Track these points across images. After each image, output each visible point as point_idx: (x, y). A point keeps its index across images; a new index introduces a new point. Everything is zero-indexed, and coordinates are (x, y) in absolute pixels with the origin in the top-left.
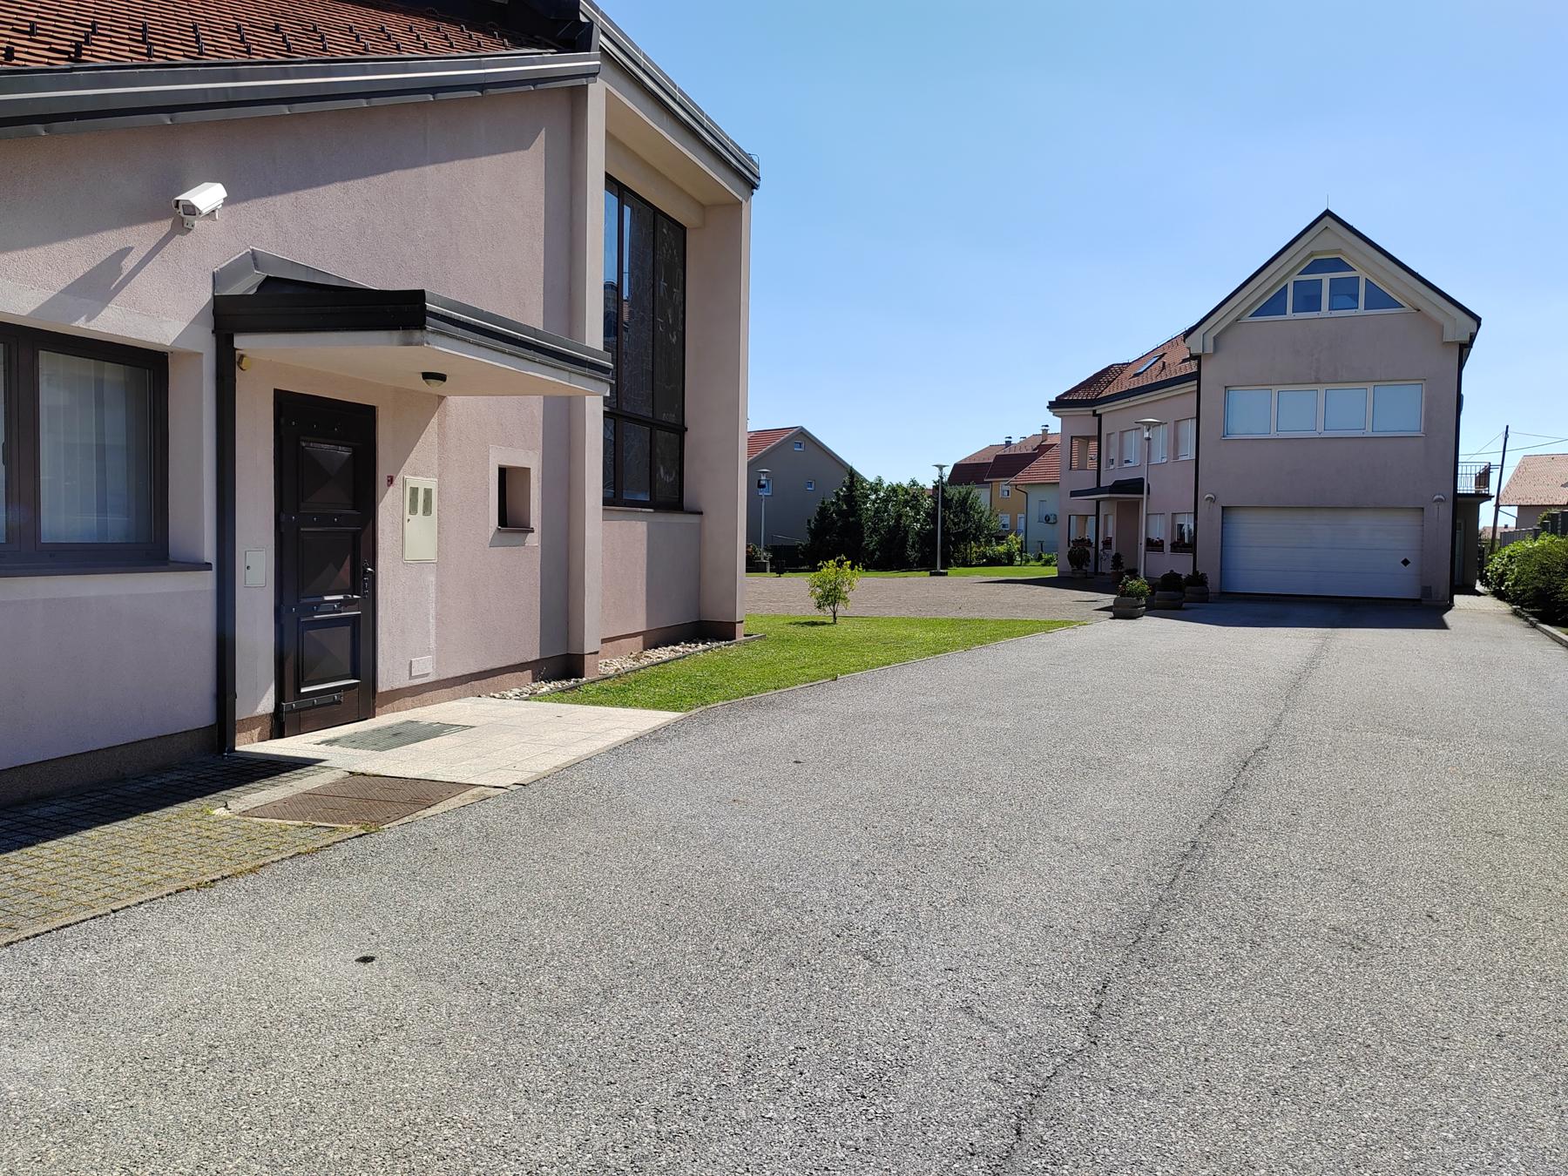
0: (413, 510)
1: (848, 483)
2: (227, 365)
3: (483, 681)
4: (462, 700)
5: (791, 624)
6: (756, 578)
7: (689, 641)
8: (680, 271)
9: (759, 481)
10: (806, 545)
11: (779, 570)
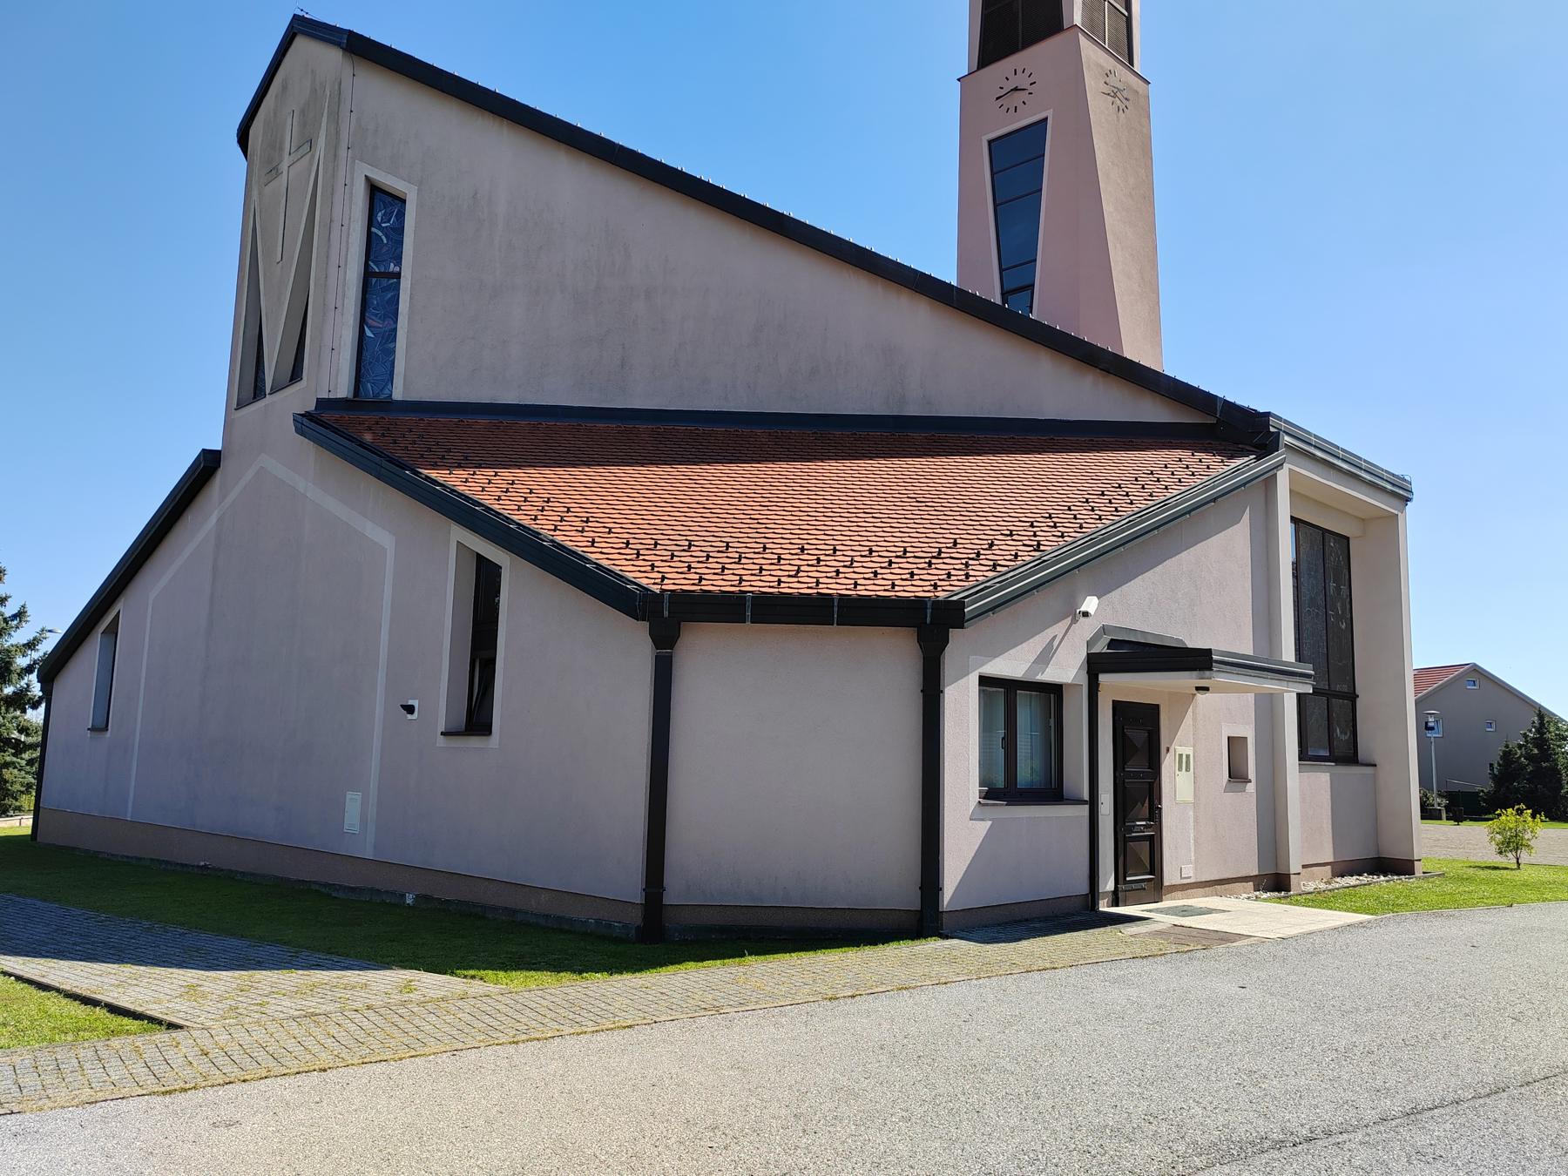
1: (1537, 724)
3: (1223, 886)
6: (1431, 825)
8: (1346, 571)
9: (1426, 723)
11: (1457, 817)
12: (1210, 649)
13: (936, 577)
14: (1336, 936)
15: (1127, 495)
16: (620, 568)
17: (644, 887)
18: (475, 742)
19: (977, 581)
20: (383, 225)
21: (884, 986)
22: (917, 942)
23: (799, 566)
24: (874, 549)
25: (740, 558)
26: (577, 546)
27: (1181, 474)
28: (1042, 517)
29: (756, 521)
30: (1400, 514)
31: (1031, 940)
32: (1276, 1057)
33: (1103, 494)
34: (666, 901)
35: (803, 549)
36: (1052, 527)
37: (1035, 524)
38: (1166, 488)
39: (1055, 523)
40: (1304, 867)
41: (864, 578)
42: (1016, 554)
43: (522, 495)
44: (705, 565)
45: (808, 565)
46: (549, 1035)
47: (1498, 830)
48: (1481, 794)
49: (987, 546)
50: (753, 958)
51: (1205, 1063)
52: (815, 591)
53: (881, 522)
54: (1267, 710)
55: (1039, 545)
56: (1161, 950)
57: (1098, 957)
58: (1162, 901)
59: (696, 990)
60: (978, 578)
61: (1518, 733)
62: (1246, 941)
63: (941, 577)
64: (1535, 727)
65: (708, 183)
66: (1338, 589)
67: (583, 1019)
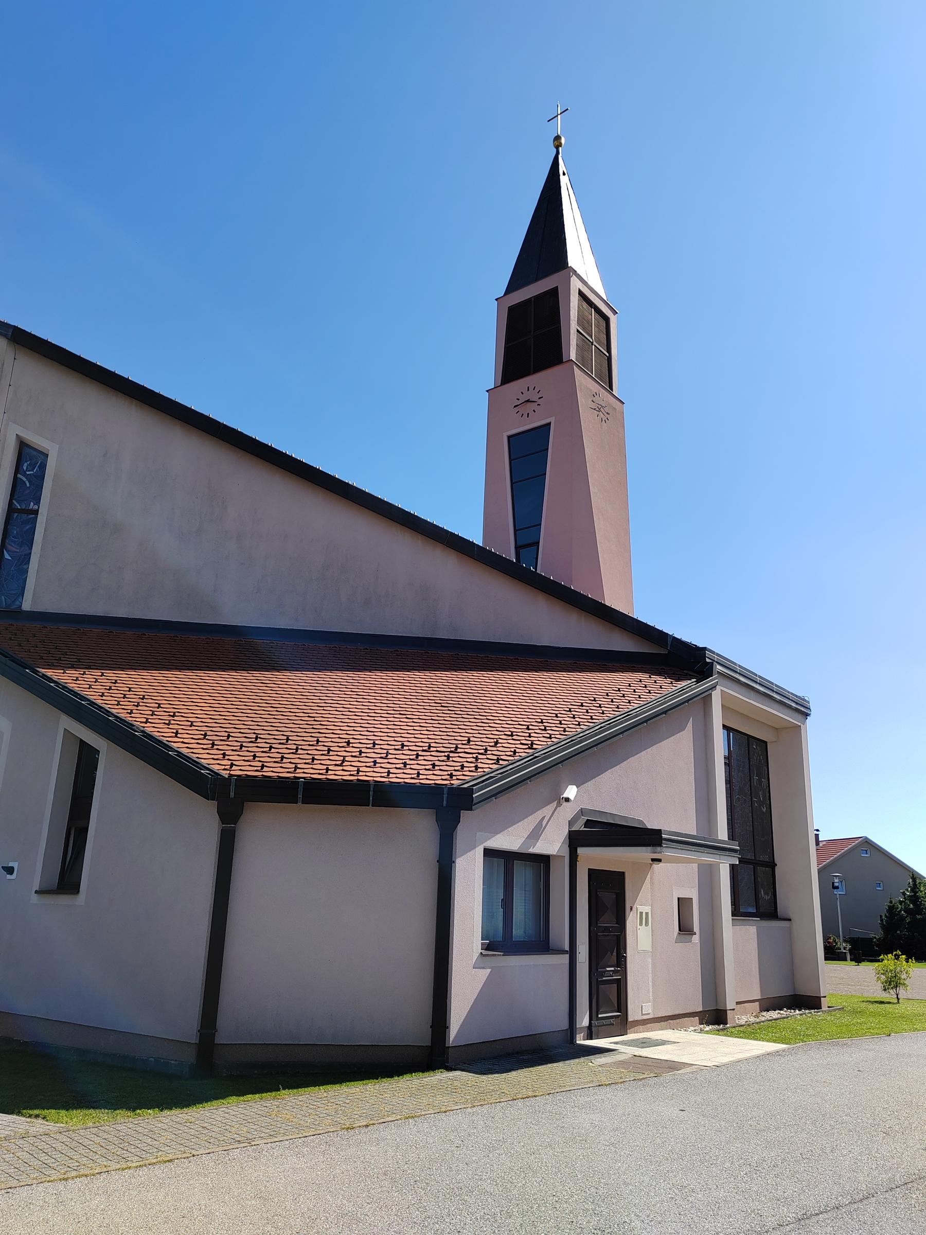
0: (641, 924)
2: (573, 858)
4: (666, 1031)
5: (863, 1001)
7: (789, 1008)
9: (833, 883)
10: (880, 939)
11: (858, 959)
12: (661, 830)
13: (453, 768)
14: (758, 1063)
15: (600, 707)
16: (197, 755)
17: (199, 1029)
18: (64, 900)
19: (484, 772)
20: (28, 473)
21: (394, 1116)
22: (426, 1074)
23: (344, 757)
24: (405, 743)
25: (297, 749)
26: (163, 736)
27: (641, 691)
28: (536, 722)
29: (313, 719)
30: (802, 725)
31: (519, 1071)
32: (703, 1172)
33: (582, 706)
34: (218, 1040)
35: (348, 743)
36: (543, 730)
37: (530, 727)
38: (629, 702)
39: (545, 727)
40: (738, 1003)
41: (396, 768)
42: (515, 750)
43: (122, 692)
44: (268, 755)
45: (352, 756)
46: (96, 1171)
47: (882, 971)
48: (875, 940)
49: (493, 744)
50: (286, 1092)
51: (646, 1179)
52: (356, 778)
53: (413, 722)
54: (707, 878)
55: (532, 744)
56: (621, 1078)
57: (570, 1086)
58: (627, 1035)
59: (233, 1124)
60: (485, 770)
61: (899, 892)
62: (689, 1069)
63: (456, 768)
64: (910, 887)
65: (291, 457)
66: (760, 781)
67: (130, 1155)
